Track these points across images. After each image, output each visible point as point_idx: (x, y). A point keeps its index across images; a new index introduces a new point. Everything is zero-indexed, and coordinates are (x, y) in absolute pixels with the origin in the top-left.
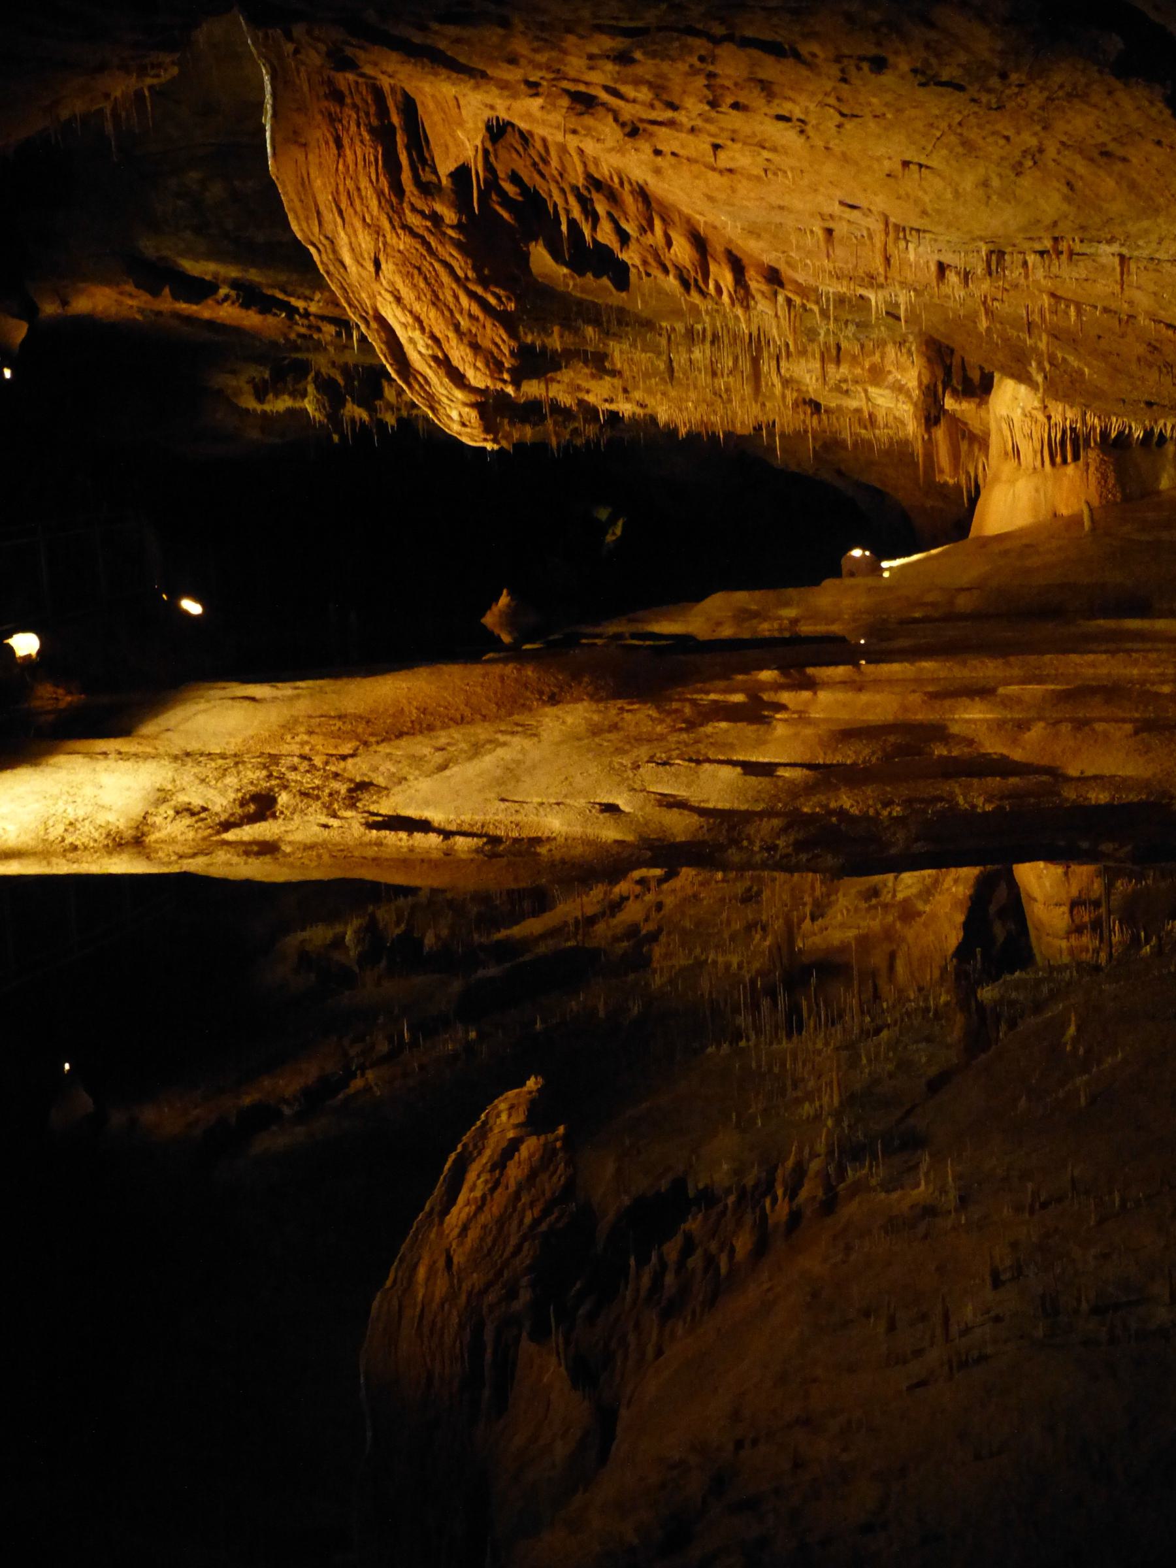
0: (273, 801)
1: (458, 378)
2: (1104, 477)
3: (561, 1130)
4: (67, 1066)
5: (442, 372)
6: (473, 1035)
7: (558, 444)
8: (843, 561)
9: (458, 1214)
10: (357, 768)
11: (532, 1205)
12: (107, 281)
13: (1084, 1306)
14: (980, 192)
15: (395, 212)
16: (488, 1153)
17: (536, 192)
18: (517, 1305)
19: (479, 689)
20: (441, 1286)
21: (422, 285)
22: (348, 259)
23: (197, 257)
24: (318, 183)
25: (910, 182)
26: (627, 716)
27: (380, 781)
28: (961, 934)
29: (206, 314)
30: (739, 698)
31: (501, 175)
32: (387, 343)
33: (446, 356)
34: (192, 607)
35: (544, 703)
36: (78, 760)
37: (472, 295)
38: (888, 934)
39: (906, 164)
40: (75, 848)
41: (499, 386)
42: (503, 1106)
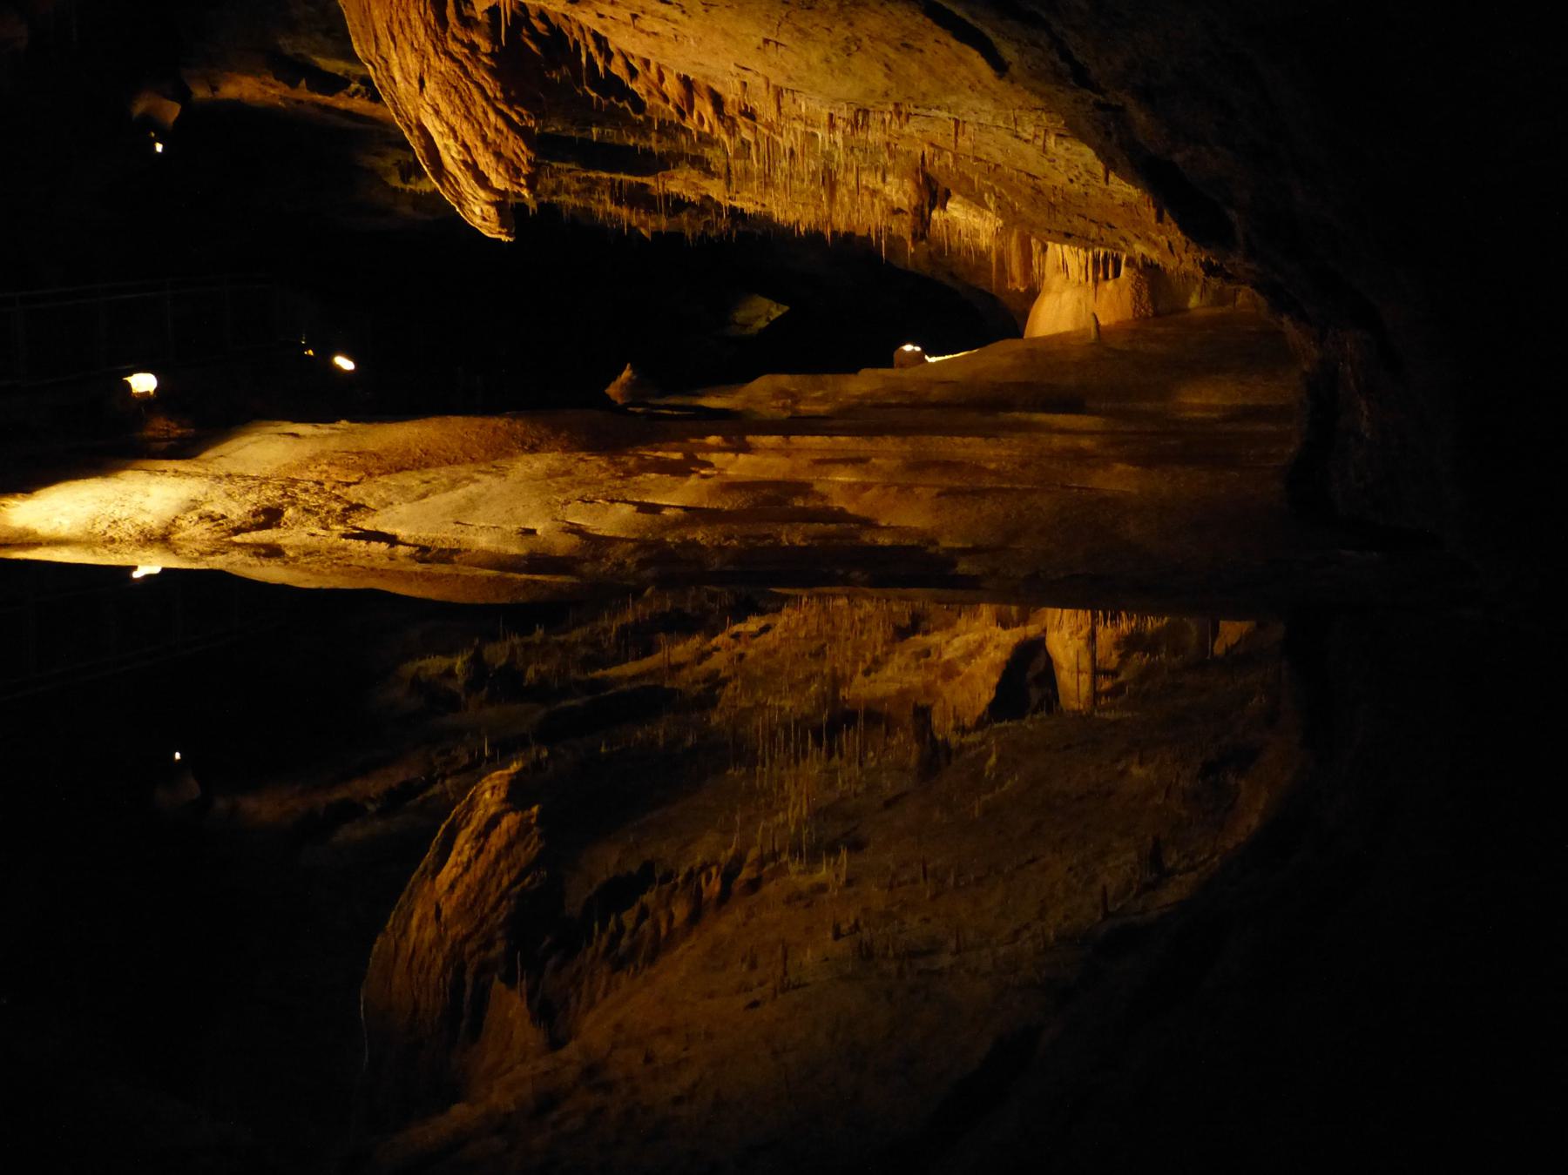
0: (282, 513)
1: (482, 180)
2: (1139, 292)
3: (535, 809)
4: (178, 756)
5: (469, 175)
6: (545, 754)
7: (694, 235)
8: (896, 354)
9: (448, 873)
10: (354, 494)
11: (509, 869)
12: (250, 72)
13: (891, 952)
14: (824, 66)
15: (438, 41)
16: (474, 823)
17: (560, 29)
18: (493, 953)
19: (474, 438)
20: (430, 932)
21: (458, 101)
22: (397, 76)
23: (326, 56)
24: (376, 13)
25: (772, 54)
26: (582, 465)
27: (372, 504)
28: (993, 694)
29: (341, 105)
30: (677, 456)
31: (532, 13)
32: (425, 148)
33: (475, 162)
34: (344, 363)
35: (526, 452)
36: (142, 474)
37: (498, 112)
38: (928, 690)
39: (766, 41)
40: (112, 540)
41: (517, 188)
42: (488, 785)
